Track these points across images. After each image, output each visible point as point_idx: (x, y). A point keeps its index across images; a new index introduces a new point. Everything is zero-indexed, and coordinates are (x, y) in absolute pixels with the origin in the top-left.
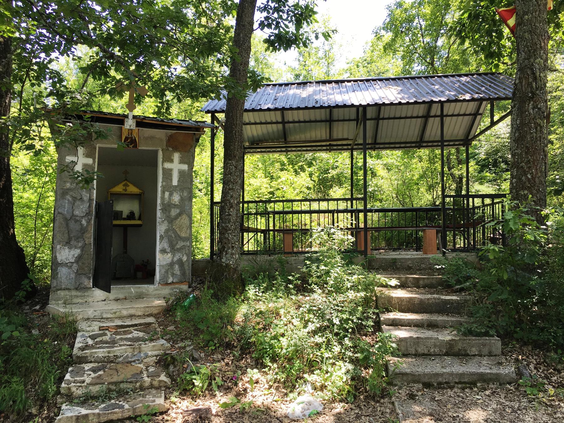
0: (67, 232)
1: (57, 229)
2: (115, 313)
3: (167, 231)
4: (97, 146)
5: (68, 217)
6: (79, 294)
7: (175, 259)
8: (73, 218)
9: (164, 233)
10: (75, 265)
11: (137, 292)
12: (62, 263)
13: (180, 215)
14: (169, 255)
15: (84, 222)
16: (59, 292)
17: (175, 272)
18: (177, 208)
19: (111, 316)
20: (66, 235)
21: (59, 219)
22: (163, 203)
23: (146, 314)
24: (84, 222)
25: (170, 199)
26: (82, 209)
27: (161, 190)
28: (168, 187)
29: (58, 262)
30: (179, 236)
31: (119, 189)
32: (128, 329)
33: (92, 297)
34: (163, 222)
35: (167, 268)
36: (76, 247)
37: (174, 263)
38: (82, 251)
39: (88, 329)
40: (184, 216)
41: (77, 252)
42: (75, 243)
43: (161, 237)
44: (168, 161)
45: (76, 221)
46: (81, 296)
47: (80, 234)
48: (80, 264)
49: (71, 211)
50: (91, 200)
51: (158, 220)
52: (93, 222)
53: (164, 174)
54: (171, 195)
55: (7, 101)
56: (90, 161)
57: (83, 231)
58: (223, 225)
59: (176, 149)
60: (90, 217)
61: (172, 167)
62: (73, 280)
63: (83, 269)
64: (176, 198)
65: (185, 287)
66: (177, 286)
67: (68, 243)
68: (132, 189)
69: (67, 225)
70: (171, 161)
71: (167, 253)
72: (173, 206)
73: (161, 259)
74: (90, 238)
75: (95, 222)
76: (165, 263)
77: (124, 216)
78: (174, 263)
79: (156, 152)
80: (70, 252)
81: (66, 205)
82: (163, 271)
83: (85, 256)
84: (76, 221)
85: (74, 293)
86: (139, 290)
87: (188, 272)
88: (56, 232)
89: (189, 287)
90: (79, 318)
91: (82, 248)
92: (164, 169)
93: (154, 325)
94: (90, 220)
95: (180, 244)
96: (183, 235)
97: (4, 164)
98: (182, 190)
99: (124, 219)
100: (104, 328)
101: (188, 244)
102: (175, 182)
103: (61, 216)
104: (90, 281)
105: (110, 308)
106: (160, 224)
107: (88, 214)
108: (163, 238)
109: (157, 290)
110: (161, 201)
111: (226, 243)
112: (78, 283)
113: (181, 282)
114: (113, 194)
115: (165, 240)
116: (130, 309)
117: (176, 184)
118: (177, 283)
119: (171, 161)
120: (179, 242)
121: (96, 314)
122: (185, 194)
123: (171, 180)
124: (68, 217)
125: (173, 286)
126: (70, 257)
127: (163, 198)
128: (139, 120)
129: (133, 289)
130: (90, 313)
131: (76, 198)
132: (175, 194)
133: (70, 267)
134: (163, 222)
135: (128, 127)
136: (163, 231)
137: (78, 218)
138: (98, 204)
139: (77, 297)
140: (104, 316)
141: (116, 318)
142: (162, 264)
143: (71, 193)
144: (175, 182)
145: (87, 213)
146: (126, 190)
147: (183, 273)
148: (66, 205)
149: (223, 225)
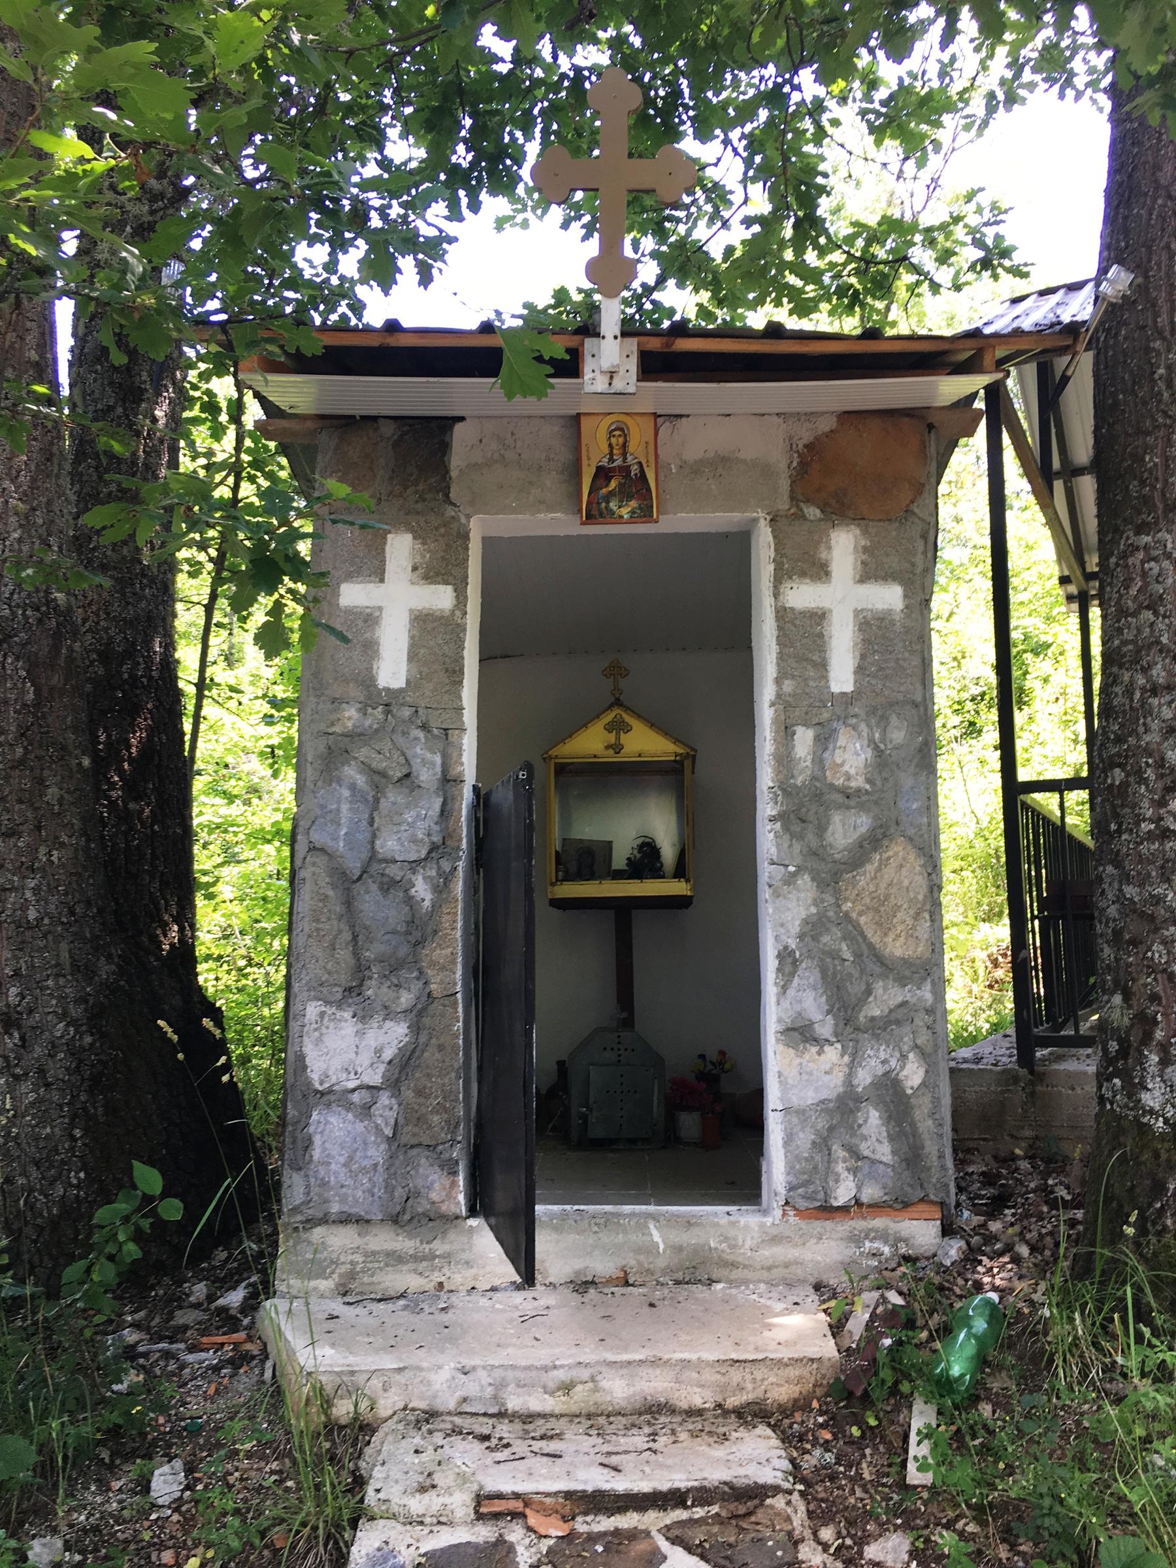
0: (347, 936)
1: (304, 926)
2: (567, 1388)
3: (813, 929)
4: (477, 528)
5: (354, 866)
6: (404, 1244)
7: (863, 1078)
8: (375, 868)
9: (801, 937)
10: (385, 1099)
11: (679, 1249)
12: (330, 1091)
13: (874, 842)
14: (832, 1054)
15: (422, 890)
16: (318, 1233)
17: (864, 1149)
18: (862, 807)
19: (548, 1404)
20: (344, 955)
21: (315, 872)
22: (785, 788)
23: (732, 1402)
24: (422, 890)
25: (819, 761)
26: (411, 825)
27: (775, 721)
28: (809, 706)
29: (309, 1083)
30: (879, 958)
31: (591, 742)
32: (627, 1521)
33: (468, 1264)
34: (790, 879)
35: (822, 1124)
36: (389, 1014)
37: (858, 1100)
38: (416, 1029)
39: (416, 1505)
40: (898, 850)
41: (393, 1035)
42: (386, 993)
43: (785, 955)
44: (803, 574)
45: (389, 886)
46: (417, 1258)
47: (403, 951)
48: (408, 1094)
49: (363, 836)
50: (449, 781)
51: (766, 872)
52: (459, 887)
53: (783, 640)
54: (824, 740)
55: (159, 413)
56: (441, 598)
57: (419, 930)
58: (1130, 891)
59: (839, 510)
60: (446, 866)
61: (826, 604)
62: (379, 1178)
63: (420, 1120)
64: (852, 758)
65: (923, 1233)
66: (879, 1223)
67: (352, 993)
68: (645, 743)
69: (349, 903)
70: (820, 571)
71: (820, 1043)
72: (840, 798)
73: (792, 1074)
74: (447, 967)
75: (471, 888)
76: (810, 1097)
77: (619, 861)
78: (858, 1100)
79: (741, 540)
80: (360, 1034)
81: (345, 807)
82: (805, 1139)
83: (431, 1056)
84: (389, 886)
85: (384, 1240)
86: (690, 1238)
87: (937, 1143)
88: (300, 940)
89: (947, 1230)
90: (385, 1407)
91: (418, 1017)
92: (782, 613)
93: (779, 1502)
94: (448, 878)
95: (885, 998)
96: (897, 948)
97: (149, 660)
98: (879, 714)
99: (618, 875)
100: (498, 1506)
101: (926, 994)
102: (842, 676)
103: (321, 860)
104: (454, 1184)
105: (542, 1355)
106: (777, 895)
107: (439, 850)
108: (795, 963)
109: (775, 1240)
110: (778, 772)
111: (1155, 998)
112: (400, 1193)
113: (899, 1204)
114: (565, 771)
115: (808, 975)
116: (644, 1371)
117: (849, 687)
118: (876, 1207)
119: (820, 571)
120: (879, 986)
121: (471, 1387)
122: (898, 735)
123: (823, 666)
124: (354, 866)
125: (860, 1224)
126: (365, 1059)
127: (784, 760)
128: (654, 344)
129: (661, 1228)
130: (441, 1380)
131: (383, 774)
132: (844, 737)
133: (366, 1111)
134: (790, 879)
135: (601, 385)
136: (795, 928)
137: (394, 871)
138: (482, 799)
139: (396, 1259)
140: (513, 1403)
141: (573, 1417)
142: (795, 1101)
143: (363, 753)
144: (842, 676)
145: (434, 848)
146: (617, 748)
147: (911, 1158)
148: (345, 807)
149: (1130, 891)
